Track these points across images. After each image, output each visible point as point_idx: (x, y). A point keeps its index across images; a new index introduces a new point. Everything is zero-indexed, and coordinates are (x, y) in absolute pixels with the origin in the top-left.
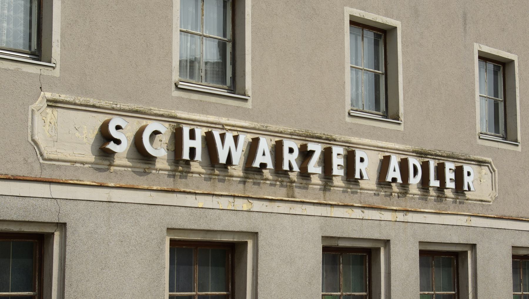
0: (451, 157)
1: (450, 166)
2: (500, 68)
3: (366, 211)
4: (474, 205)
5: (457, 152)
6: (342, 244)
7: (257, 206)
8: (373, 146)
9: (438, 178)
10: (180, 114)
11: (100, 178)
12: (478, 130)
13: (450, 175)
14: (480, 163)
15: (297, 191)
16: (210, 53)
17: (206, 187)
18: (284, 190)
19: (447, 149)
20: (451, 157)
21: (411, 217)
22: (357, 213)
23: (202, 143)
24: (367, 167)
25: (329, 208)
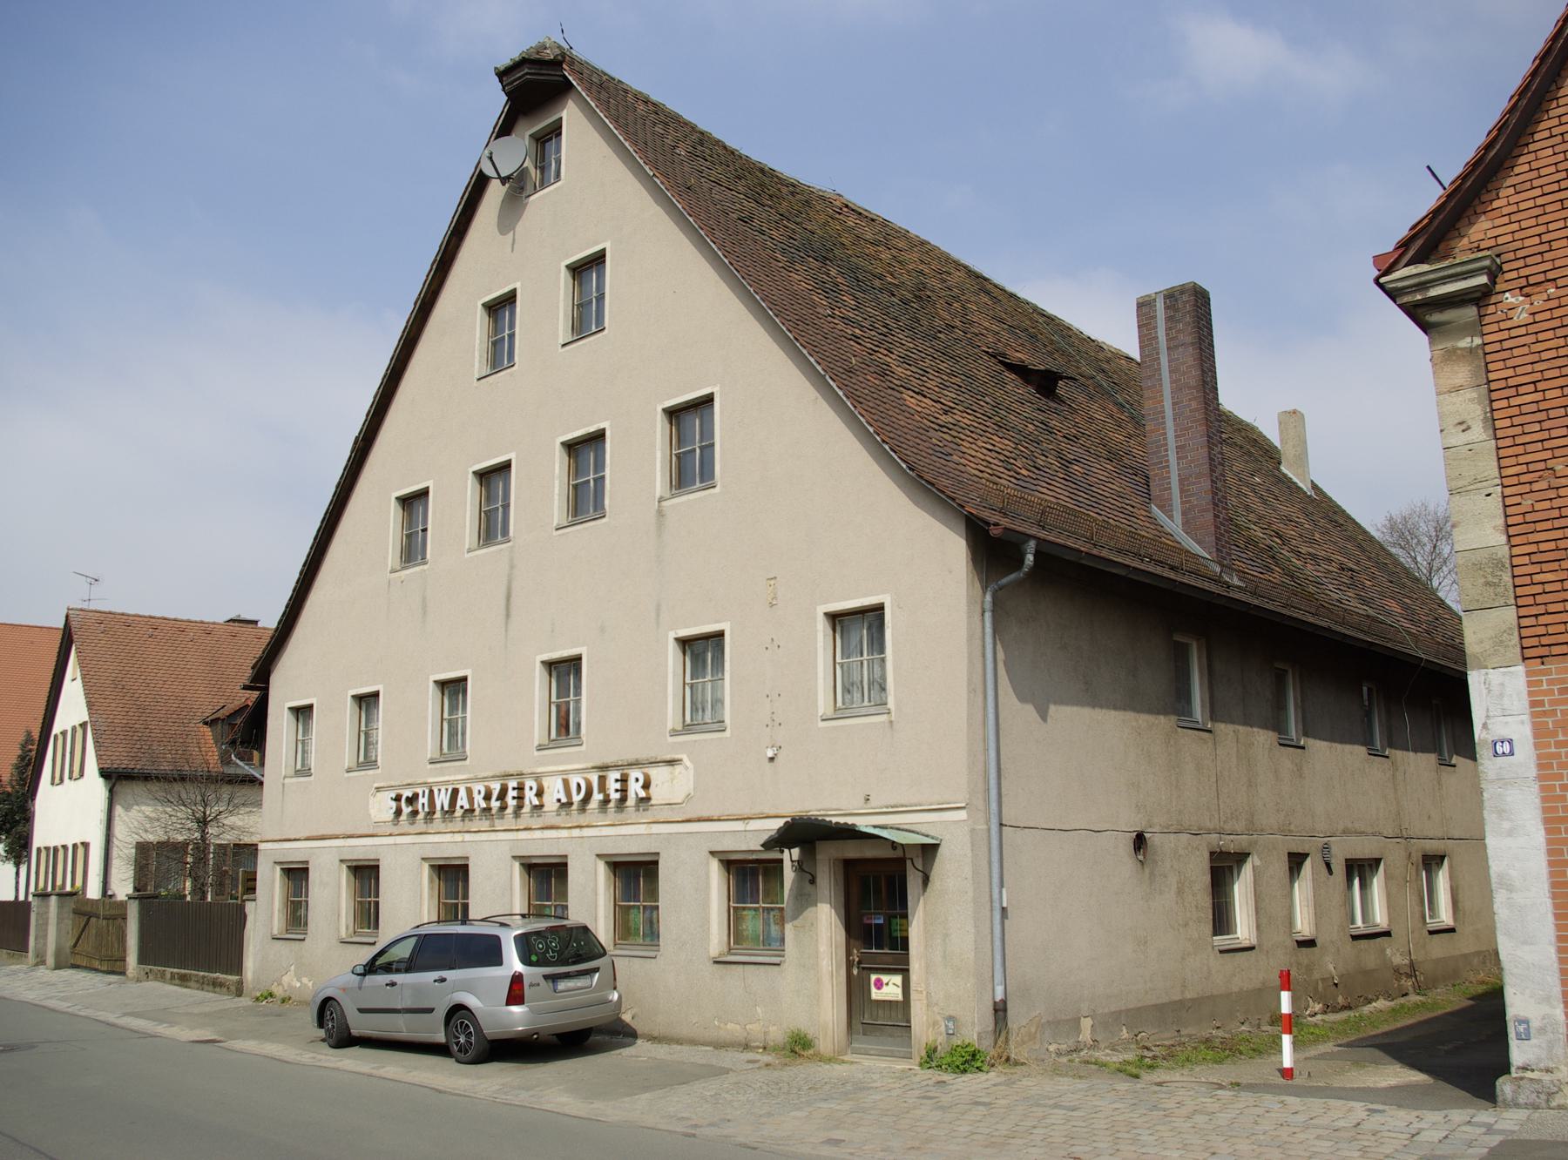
0: (635, 764)
1: (635, 774)
2: (702, 649)
5: (643, 755)
6: (534, 861)
7: (468, 837)
8: (560, 772)
10: (430, 780)
11: (396, 830)
12: (670, 726)
13: (613, 786)
14: (671, 762)
15: (497, 822)
16: (1470, 312)
17: (442, 827)
19: (631, 757)
20: (635, 764)
21: (587, 832)
22: (538, 834)
24: (554, 791)
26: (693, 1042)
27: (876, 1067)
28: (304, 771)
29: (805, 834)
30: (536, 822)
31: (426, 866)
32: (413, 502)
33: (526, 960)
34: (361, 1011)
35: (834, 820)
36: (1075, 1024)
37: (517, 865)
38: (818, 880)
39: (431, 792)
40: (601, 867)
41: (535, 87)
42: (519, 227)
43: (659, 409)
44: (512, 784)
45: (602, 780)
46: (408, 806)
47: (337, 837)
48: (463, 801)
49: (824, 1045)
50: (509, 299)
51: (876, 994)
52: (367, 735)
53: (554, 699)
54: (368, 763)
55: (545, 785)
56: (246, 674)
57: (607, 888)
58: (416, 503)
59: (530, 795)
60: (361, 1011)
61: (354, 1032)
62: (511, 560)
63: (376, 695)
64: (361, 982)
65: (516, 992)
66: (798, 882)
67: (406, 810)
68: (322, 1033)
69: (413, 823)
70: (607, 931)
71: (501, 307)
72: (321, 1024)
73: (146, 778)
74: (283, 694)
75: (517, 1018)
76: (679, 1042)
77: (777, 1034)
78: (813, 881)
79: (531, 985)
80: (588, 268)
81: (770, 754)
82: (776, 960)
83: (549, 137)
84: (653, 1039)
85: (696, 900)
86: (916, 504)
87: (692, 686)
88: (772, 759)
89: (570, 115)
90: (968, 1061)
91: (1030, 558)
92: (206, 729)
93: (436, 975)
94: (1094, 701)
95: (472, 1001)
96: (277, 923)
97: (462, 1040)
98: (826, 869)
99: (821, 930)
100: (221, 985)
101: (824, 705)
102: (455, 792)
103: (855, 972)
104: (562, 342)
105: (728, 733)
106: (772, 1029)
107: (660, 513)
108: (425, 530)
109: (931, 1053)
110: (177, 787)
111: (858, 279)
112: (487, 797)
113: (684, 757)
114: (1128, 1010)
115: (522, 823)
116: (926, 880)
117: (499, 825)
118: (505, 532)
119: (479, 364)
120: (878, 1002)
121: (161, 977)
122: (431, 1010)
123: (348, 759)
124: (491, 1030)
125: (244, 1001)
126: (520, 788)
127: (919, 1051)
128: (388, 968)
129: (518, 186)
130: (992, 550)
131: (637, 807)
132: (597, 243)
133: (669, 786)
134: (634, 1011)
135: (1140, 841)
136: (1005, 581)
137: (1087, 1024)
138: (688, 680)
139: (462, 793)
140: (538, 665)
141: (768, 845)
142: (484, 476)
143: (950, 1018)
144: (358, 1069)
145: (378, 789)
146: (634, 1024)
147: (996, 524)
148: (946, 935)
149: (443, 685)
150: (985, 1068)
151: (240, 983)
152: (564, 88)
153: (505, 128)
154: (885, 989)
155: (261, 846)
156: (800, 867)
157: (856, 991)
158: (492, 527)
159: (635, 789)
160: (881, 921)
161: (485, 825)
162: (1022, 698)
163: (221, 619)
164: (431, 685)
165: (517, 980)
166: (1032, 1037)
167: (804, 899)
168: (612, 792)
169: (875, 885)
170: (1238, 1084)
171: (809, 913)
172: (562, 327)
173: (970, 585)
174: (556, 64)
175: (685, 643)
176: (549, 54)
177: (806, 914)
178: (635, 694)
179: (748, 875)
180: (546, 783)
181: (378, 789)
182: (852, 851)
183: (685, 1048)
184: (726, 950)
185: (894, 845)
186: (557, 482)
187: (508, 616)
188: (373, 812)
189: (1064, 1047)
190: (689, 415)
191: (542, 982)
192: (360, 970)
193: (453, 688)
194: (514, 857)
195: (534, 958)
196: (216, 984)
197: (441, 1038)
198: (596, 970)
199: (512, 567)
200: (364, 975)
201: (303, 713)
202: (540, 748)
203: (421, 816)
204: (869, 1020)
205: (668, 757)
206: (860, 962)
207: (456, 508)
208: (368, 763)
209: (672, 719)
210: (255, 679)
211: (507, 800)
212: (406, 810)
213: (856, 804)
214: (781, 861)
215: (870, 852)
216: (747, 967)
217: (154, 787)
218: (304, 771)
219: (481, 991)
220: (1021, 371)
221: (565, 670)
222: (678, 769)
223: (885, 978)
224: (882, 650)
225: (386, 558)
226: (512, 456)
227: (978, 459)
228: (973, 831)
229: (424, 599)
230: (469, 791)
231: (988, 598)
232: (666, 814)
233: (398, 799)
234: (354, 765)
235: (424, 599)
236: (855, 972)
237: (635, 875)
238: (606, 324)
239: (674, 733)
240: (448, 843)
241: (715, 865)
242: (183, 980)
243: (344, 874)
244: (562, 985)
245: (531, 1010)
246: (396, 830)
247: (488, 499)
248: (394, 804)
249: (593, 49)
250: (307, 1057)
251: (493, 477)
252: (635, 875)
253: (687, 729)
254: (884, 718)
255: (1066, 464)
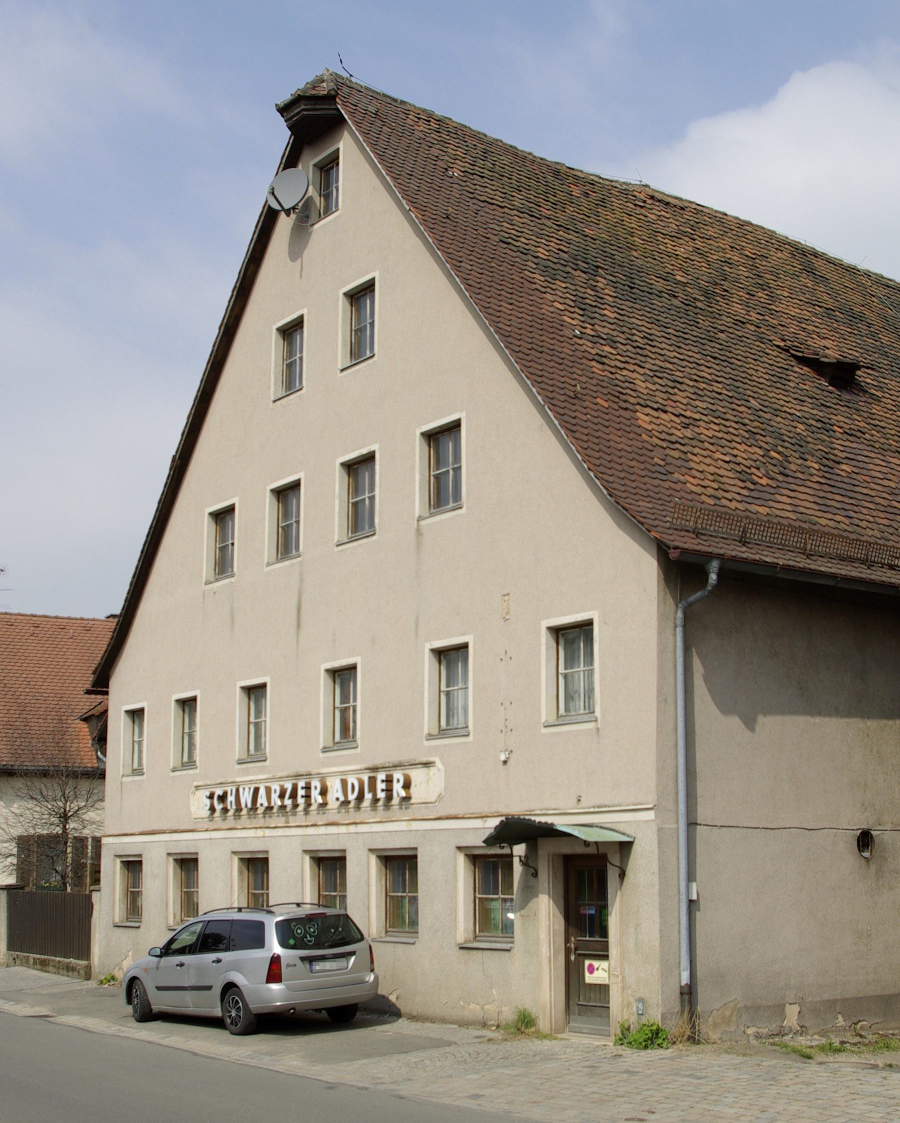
1: (398, 775)
2: (451, 657)
3: (413, 823)
4: (419, 808)
5: (404, 757)
7: (268, 832)
8: (342, 770)
9: (381, 790)
10: (238, 779)
11: (211, 826)
13: (381, 786)
14: (427, 764)
15: (291, 818)
18: (283, 819)
19: (395, 759)
21: (361, 828)
22: (322, 830)
23: (594, 494)
24: (335, 786)
25: (304, 829)
26: (444, 1021)
27: (581, 1042)
28: (138, 771)
29: (513, 830)
30: (321, 820)
31: (236, 859)
32: (223, 517)
33: (284, 944)
34: (159, 988)
35: (538, 819)
36: (780, 1011)
37: (307, 858)
38: (540, 874)
39: (237, 790)
40: (373, 860)
41: (313, 121)
42: (306, 254)
43: (418, 434)
44: (301, 784)
45: (373, 780)
46: (220, 803)
47: (163, 832)
48: (262, 799)
49: (544, 1024)
50: (368, 288)
51: (589, 978)
52: (257, 726)
53: (338, 704)
54: (190, 763)
55: (329, 784)
56: (88, 681)
57: (379, 880)
58: (442, 438)
59: (398, 788)
60: (159, 988)
61: (155, 1008)
62: (301, 574)
63: (263, 686)
64: (159, 962)
65: (274, 972)
66: (524, 875)
67: (218, 807)
68: (130, 1009)
69: (225, 819)
70: (378, 918)
71: (291, 331)
72: (129, 1001)
73: (26, 774)
74: (122, 696)
75: (276, 995)
76: (432, 1020)
77: (509, 1015)
78: (535, 875)
79: (288, 966)
80: (360, 296)
81: (503, 758)
82: (508, 946)
83: (328, 168)
84: (413, 1018)
85: (448, 890)
86: (619, 526)
87: (566, 676)
88: (505, 762)
89: (347, 147)
90: (653, 1038)
91: (713, 577)
92: (84, 726)
93: (214, 956)
94: (812, 708)
95: (239, 979)
96: (119, 913)
97: (233, 1014)
98: (546, 863)
99: (541, 919)
100: (73, 969)
101: (546, 712)
102: (256, 790)
103: (573, 958)
104: (340, 367)
105: (470, 738)
106: (505, 1009)
107: (419, 532)
108: (233, 544)
110: (38, 784)
111: (631, 287)
112: (282, 796)
113: (437, 760)
114: (844, 1000)
115: (311, 819)
116: (622, 875)
117: (293, 821)
118: (457, 496)
119: (274, 387)
120: (590, 985)
121: (26, 963)
122: (209, 988)
123: (172, 759)
124: (255, 1005)
125: (92, 984)
126: (308, 788)
127: (615, 1029)
128: (182, 951)
129: (305, 215)
130: (681, 571)
131: (400, 804)
132: (367, 273)
133: (427, 786)
134: (398, 992)
135: (865, 840)
136: (692, 598)
137: (792, 1012)
138: (443, 688)
139: (262, 792)
140: (323, 673)
141: (490, 841)
142: (433, 437)
143: (641, 1000)
144: (151, 1039)
145: (197, 788)
146: (399, 1004)
147: (676, 548)
148: (638, 925)
149: (440, 654)
150: (664, 1045)
151: (89, 968)
152: (335, 123)
153: (291, 160)
154: (596, 974)
155: (105, 841)
156: (525, 863)
157: (573, 975)
158: (286, 544)
159: (398, 789)
160: (593, 912)
161: (281, 821)
162: (725, 709)
163: (102, 617)
164: (238, 690)
165: (275, 961)
166: (727, 1021)
167: (529, 892)
168: (381, 790)
169: (585, 877)
170: (890, 1066)
171: (532, 905)
172: (341, 356)
173: (661, 602)
174: (330, 98)
175: (557, 632)
176: (324, 89)
177: (531, 905)
178: (398, 701)
179: (488, 865)
180: (329, 782)
181: (197, 788)
182: (566, 849)
183: (428, 1025)
184: (472, 937)
185: (586, 844)
186: (337, 501)
187: (299, 626)
188: (193, 809)
189: (765, 1031)
190: (443, 437)
191: (299, 962)
192: (158, 952)
193: (255, 692)
194: (305, 851)
195: (292, 942)
196: (70, 969)
197: (218, 1012)
198: (352, 953)
199: (302, 581)
200: (160, 956)
201: (136, 715)
202: (325, 750)
203: (231, 813)
204: (583, 1000)
205: (424, 760)
206: (576, 949)
207: (257, 522)
208: (190, 763)
209: (428, 724)
210: (96, 684)
211: (297, 798)
212: (218, 807)
213: (569, 804)
214: (511, 856)
215: (580, 850)
216: (485, 952)
217: (19, 783)
218: (138, 771)
219: (244, 968)
220: (815, 364)
221: (343, 676)
222: (432, 770)
223: (596, 964)
224: (592, 663)
225: (201, 570)
226: (300, 475)
227: (711, 476)
228: (660, 830)
229: (232, 609)
230: (268, 790)
231: (680, 614)
232: (424, 812)
233: (211, 797)
234: (179, 764)
235: (232, 609)
236: (573, 958)
237: (400, 865)
238: (376, 351)
239: (430, 737)
240: (252, 837)
241: (461, 859)
242: (43, 965)
243: (171, 866)
244: (318, 966)
245: (288, 987)
246: (211, 826)
247: (438, 464)
248: (208, 802)
249: (380, 72)
250: (114, 1029)
251: (359, 468)
252: (400, 865)
253: (442, 733)
254: (592, 725)
255: (829, 462)
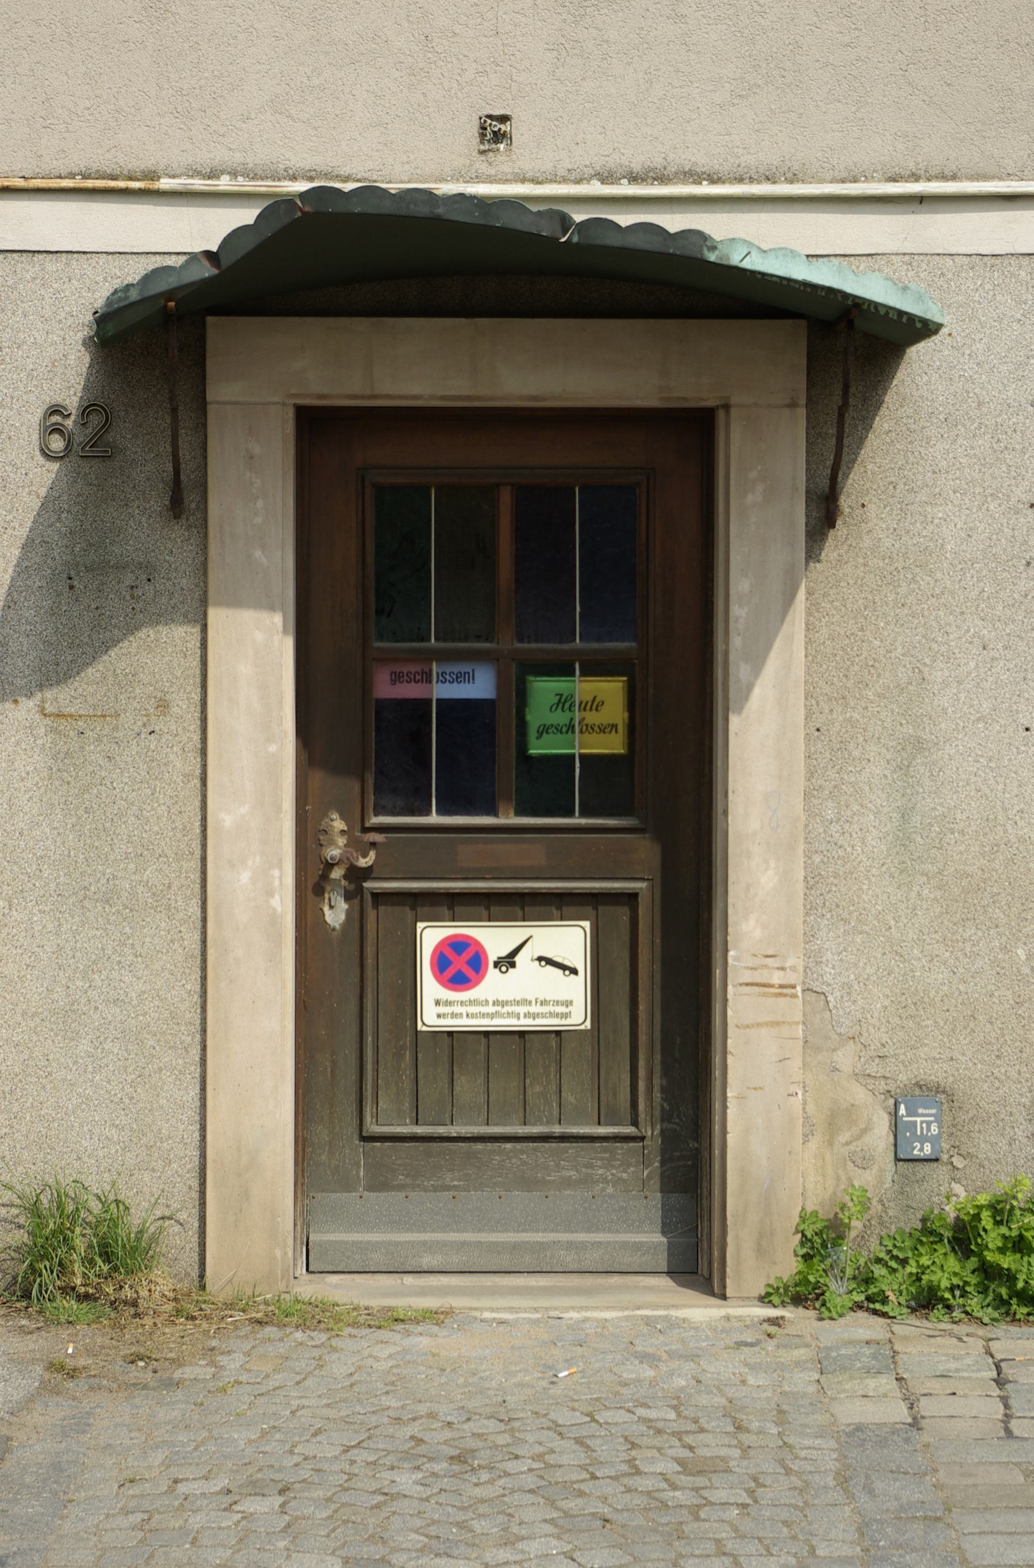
27: (538, 1322)
51: (438, 1007)
103: (336, 913)
109: (821, 1241)
116: (824, 511)
120: (454, 1042)
154: (493, 984)
223: (494, 938)
